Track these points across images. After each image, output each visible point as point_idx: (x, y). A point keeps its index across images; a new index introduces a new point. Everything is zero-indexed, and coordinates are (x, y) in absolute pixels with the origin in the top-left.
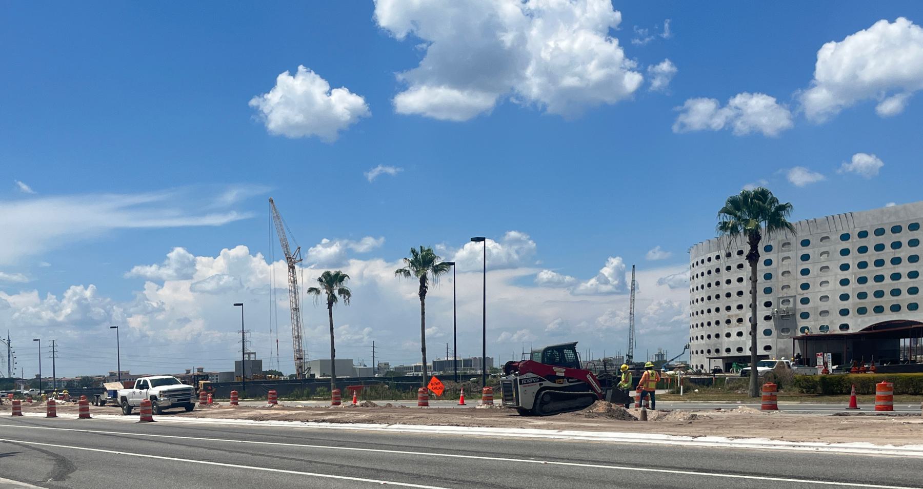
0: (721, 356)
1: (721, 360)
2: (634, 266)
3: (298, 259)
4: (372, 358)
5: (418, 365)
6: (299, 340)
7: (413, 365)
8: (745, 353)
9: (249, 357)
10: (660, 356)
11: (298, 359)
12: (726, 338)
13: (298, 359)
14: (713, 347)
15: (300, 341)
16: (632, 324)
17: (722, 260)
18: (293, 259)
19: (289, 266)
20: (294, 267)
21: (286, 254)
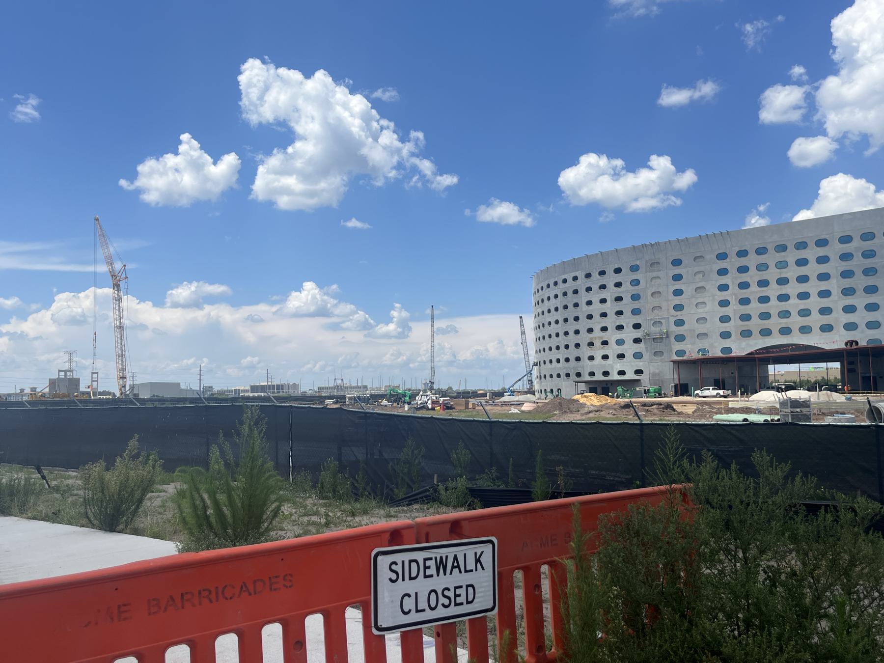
0: (583, 380)
1: (584, 384)
2: (432, 306)
3: (124, 276)
4: (199, 381)
5: (237, 388)
6: (122, 358)
7: (233, 388)
9: (66, 375)
11: (121, 378)
12: (589, 361)
13: (121, 378)
15: (124, 360)
17: (579, 282)
18: (118, 276)
19: (113, 284)
20: (119, 285)
21: (111, 272)
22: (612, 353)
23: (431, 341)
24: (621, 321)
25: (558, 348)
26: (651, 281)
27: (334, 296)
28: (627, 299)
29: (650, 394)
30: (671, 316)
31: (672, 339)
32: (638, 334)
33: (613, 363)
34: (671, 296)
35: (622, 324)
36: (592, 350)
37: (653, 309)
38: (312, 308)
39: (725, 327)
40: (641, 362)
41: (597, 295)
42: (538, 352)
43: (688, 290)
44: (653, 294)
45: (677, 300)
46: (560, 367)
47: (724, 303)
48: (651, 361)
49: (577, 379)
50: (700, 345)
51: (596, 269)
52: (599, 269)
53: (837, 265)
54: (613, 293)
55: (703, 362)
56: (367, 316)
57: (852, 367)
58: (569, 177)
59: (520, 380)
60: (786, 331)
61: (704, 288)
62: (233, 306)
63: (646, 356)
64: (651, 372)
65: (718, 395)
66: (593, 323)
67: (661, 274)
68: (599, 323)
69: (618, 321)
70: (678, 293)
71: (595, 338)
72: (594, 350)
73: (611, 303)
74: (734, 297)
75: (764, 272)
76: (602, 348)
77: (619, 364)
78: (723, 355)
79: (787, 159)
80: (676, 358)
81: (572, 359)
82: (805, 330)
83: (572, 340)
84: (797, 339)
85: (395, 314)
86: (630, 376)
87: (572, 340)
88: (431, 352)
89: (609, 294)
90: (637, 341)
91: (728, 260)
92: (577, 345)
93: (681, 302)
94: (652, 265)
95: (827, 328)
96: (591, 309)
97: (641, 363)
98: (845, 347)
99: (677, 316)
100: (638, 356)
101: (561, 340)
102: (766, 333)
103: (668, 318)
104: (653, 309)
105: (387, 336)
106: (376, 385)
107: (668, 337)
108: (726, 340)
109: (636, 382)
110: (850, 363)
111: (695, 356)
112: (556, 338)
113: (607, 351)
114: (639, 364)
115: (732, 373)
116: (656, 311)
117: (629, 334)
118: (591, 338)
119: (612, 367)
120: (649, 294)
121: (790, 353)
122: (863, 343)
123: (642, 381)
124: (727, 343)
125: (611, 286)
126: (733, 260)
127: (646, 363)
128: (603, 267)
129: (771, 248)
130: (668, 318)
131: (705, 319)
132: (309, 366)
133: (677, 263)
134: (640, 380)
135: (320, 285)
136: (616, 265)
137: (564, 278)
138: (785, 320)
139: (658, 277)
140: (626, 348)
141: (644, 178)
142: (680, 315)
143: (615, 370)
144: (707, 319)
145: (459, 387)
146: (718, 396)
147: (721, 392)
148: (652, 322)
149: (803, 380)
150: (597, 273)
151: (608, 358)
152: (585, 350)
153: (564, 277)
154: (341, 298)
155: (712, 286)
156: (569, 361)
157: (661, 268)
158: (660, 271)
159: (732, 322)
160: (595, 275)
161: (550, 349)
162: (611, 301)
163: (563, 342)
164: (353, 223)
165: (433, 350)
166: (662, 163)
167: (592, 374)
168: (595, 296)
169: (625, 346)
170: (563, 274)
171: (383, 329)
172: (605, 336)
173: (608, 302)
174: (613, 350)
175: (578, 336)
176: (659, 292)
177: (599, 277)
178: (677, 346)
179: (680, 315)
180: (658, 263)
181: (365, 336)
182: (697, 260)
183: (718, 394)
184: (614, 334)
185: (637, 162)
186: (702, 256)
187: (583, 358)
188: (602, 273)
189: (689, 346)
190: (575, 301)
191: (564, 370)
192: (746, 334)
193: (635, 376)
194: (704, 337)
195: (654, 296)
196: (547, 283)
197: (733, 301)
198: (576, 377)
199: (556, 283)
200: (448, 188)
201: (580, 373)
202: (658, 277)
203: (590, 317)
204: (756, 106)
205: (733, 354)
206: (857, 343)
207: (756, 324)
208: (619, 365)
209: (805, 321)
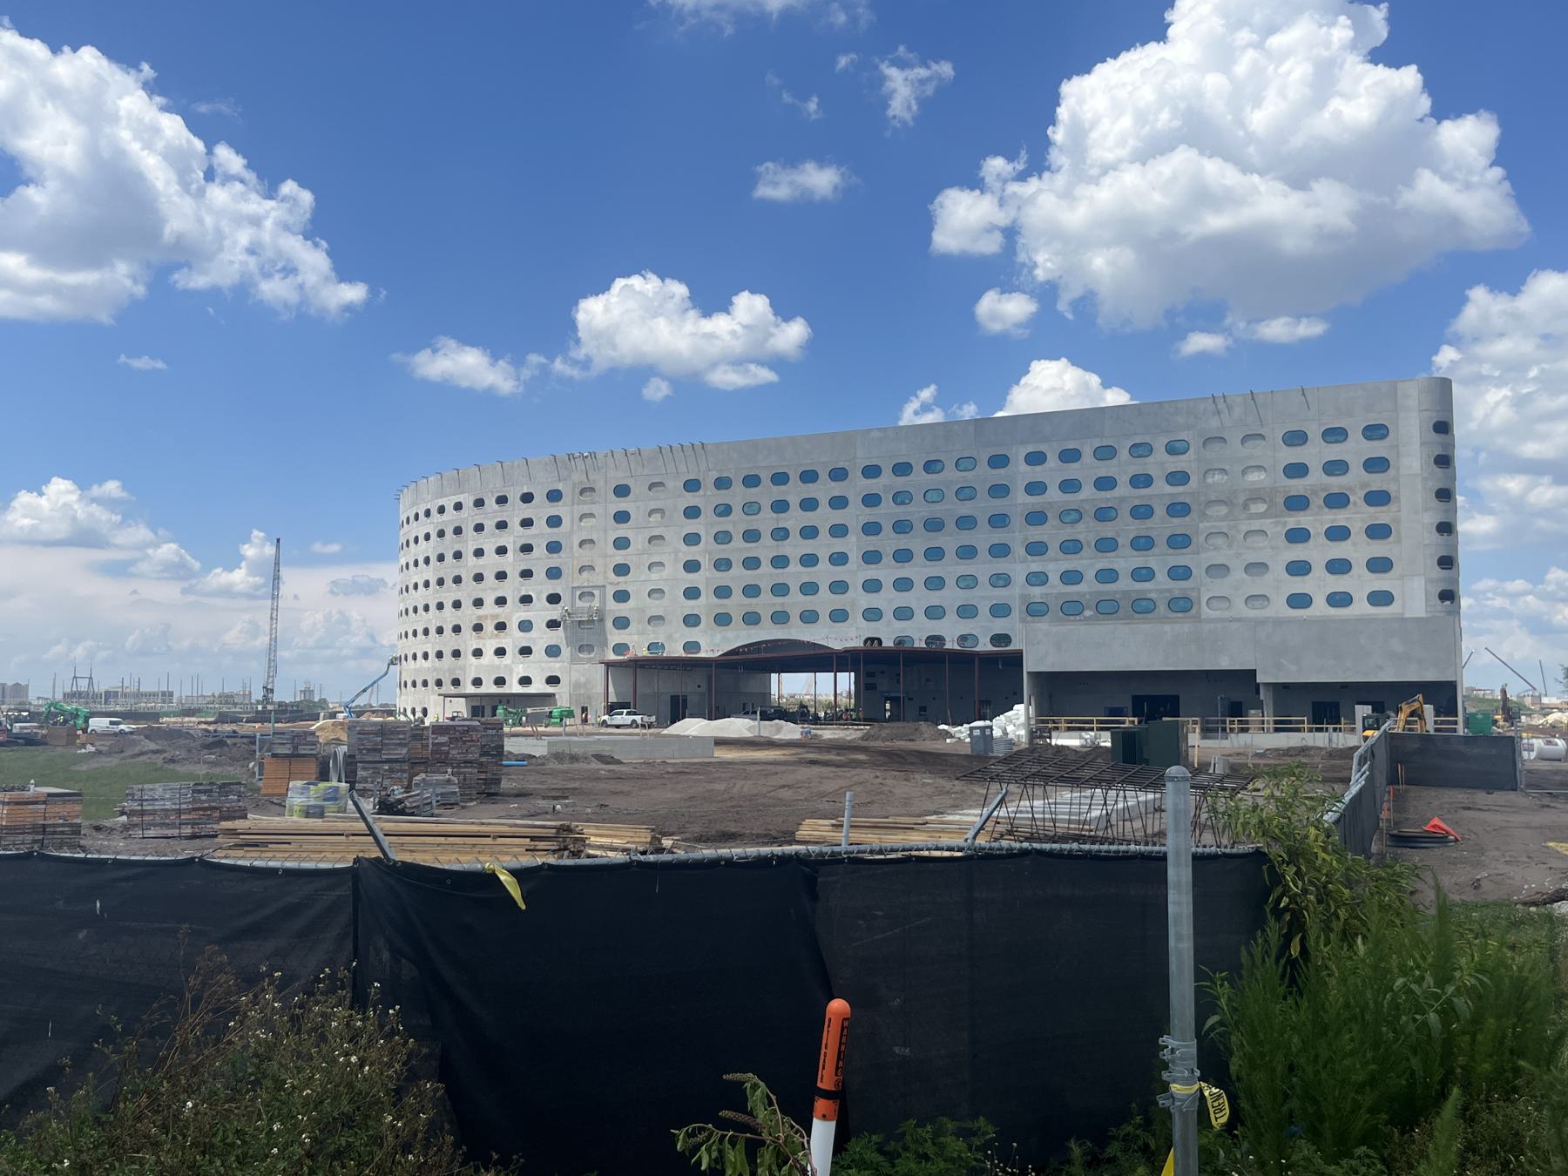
0: (463, 692)
1: (464, 699)
2: (278, 540)
8: (511, 686)
10: (307, 694)
12: (473, 658)
14: (447, 675)
16: (273, 636)
17: (464, 513)
22: (511, 645)
23: (272, 609)
24: (528, 588)
25: (440, 631)
26: (581, 519)
27: (109, 503)
28: (540, 550)
29: (553, 720)
30: (610, 584)
31: (609, 624)
32: (555, 612)
33: (513, 662)
34: (611, 549)
35: (531, 593)
36: (479, 638)
37: (581, 570)
38: (62, 530)
39: (692, 606)
40: (557, 662)
41: (493, 540)
42: (403, 637)
43: (638, 540)
44: (582, 544)
45: (620, 557)
46: (428, 668)
47: (692, 566)
48: (573, 661)
49: (452, 690)
50: (652, 636)
51: (492, 492)
52: (497, 492)
53: (858, 513)
54: (517, 537)
55: (642, 666)
56: (183, 551)
57: (871, 680)
58: (593, 312)
59: (364, 691)
60: (780, 618)
61: (661, 537)
62: (1491, 291)
63: (566, 652)
64: (573, 679)
65: (634, 724)
66: (482, 590)
67: (594, 509)
68: (494, 589)
69: (523, 588)
70: (622, 543)
71: (486, 617)
72: (484, 639)
73: (514, 555)
74: (707, 556)
75: (754, 517)
76: (497, 635)
77: (521, 666)
78: (959, 648)
79: (973, 315)
80: (612, 657)
81: (447, 653)
82: (809, 617)
83: (449, 619)
84: (797, 632)
85: (249, 551)
86: (538, 687)
87: (449, 619)
88: (271, 629)
89: (511, 540)
90: (553, 624)
91: (701, 492)
92: (478, 628)
93: (625, 560)
94: (582, 492)
95: (839, 616)
96: (481, 563)
97: (558, 665)
98: (925, 646)
99: (618, 583)
100: (553, 651)
101: (431, 617)
102: (780, 618)
103: (604, 586)
104: (581, 570)
105: (227, 592)
106: (187, 692)
107: (601, 620)
108: (693, 629)
109: (548, 698)
110: (870, 674)
111: (644, 653)
112: (424, 613)
113: (503, 641)
114: (555, 667)
115: (699, 686)
116: (585, 574)
117: (541, 612)
118: (479, 617)
119: (511, 671)
120: (576, 543)
121: (763, 655)
122: (888, 643)
123: (557, 696)
124: (694, 634)
125: (514, 523)
126: (709, 493)
127: (566, 664)
128: (504, 489)
129: (765, 477)
130: (604, 586)
131: (661, 591)
132: (59, 649)
133: (622, 491)
134: (554, 695)
135: (83, 484)
136: (525, 488)
137: (440, 504)
138: (780, 600)
139: (592, 515)
140: (534, 636)
141: (720, 325)
142: (623, 583)
143: (515, 675)
144: (664, 593)
145: (370, 700)
146: (634, 725)
147: (638, 718)
148: (578, 593)
149: (820, 701)
150: (494, 500)
151: (505, 654)
152: (468, 637)
153: (441, 502)
154: (127, 512)
155: (674, 536)
156: (459, 656)
157: (597, 499)
158: (595, 503)
159: (702, 599)
160: (490, 502)
161: (426, 632)
162: (515, 551)
163: (434, 621)
164: (143, 363)
165: (274, 626)
166: (750, 306)
167: (477, 682)
168: (489, 543)
169: (533, 634)
170: (441, 497)
171: (221, 577)
172: (502, 613)
173: (510, 553)
174: (513, 639)
175: (459, 613)
176: (592, 541)
177: (496, 507)
178: (615, 637)
179: (623, 583)
180: (592, 490)
181: (184, 592)
182: (654, 489)
183: (634, 721)
184: (517, 612)
185: (710, 300)
186: (661, 483)
187: (465, 653)
188: (502, 500)
189: (635, 637)
190: (457, 547)
191: (435, 674)
192: (723, 620)
193: (547, 686)
194: (657, 622)
195: (583, 547)
196: (415, 512)
197: (706, 563)
198: (452, 688)
199: (442, 510)
200: (349, 308)
201: (458, 679)
202: (592, 515)
203: (501, 576)
204: (927, 223)
205: (702, 655)
206: (880, 641)
207: (736, 604)
208: (521, 668)
209: (839, 601)
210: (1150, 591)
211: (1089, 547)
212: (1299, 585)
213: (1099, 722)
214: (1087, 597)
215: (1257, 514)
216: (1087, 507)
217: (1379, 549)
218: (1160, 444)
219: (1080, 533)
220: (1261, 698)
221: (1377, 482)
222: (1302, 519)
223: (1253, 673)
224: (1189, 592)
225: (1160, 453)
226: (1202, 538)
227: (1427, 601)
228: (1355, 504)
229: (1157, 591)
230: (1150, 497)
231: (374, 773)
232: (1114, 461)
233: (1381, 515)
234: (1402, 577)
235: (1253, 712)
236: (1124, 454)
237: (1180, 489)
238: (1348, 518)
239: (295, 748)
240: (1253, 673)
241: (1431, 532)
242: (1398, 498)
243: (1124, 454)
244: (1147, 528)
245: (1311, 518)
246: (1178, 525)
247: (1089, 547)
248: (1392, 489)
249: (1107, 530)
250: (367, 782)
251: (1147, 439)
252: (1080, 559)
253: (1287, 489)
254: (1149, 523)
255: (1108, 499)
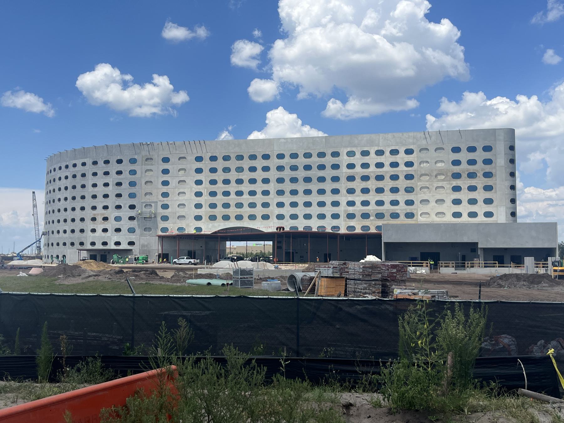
210: (397, 210)
211: (373, 191)
212: (457, 209)
213: (413, 263)
214: (372, 211)
215: (441, 180)
216: (372, 174)
217: (488, 195)
218: (402, 150)
219: (369, 185)
220: (479, 254)
221: (488, 168)
222: (458, 182)
223: (476, 244)
224: (413, 210)
225: (402, 154)
226: (419, 188)
227: (506, 216)
228: (479, 177)
229: (400, 210)
230: (398, 171)
231: (369, 285)
232: (383, 156)
233: (489, 182)
234: (497, 206)
235: (475, 259)
236: (387, 153)
237: (410, 169)
238: (476, 182)
239: (341, 274)
240: (476, 244)
241: (508, 189)
242: (496, 175)
243: (387, 153)
244: (397, 184)
245: (462, 182)
246: (409, 183)
247: (373, 191)
248: (493, 172)
249: (380, 184)
250: (366, 289)
251: (397, 148)
252: (369, 196)
253: (453, 170)
254: (397, 182)
255: (380, 172)
